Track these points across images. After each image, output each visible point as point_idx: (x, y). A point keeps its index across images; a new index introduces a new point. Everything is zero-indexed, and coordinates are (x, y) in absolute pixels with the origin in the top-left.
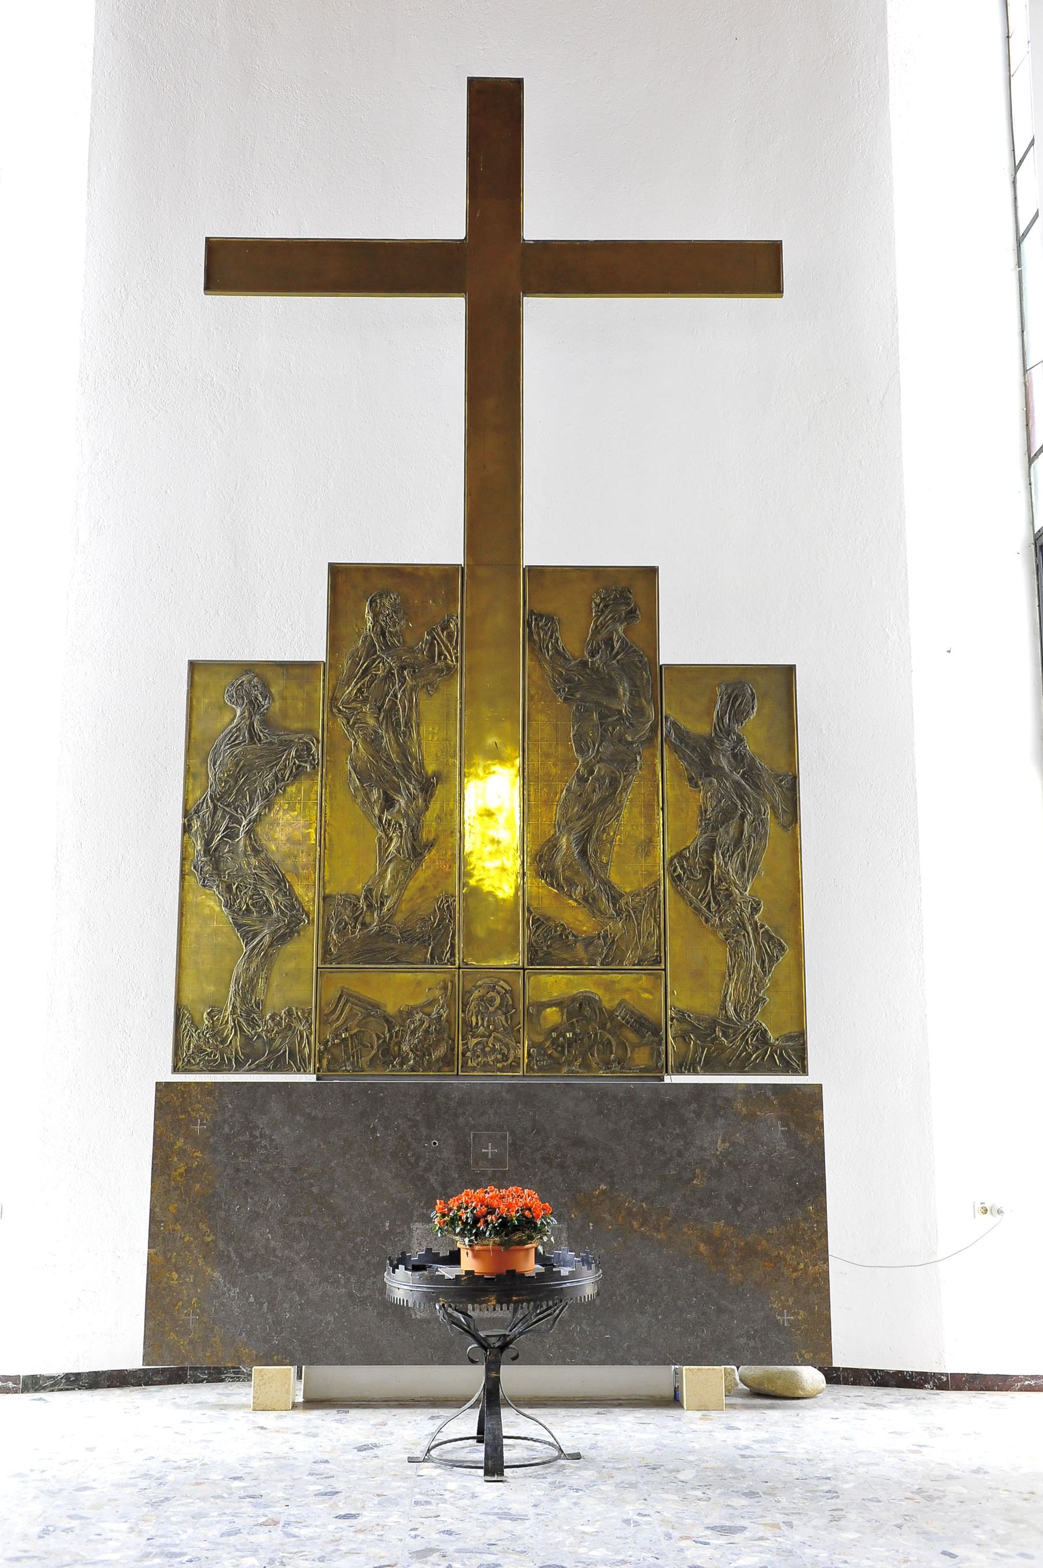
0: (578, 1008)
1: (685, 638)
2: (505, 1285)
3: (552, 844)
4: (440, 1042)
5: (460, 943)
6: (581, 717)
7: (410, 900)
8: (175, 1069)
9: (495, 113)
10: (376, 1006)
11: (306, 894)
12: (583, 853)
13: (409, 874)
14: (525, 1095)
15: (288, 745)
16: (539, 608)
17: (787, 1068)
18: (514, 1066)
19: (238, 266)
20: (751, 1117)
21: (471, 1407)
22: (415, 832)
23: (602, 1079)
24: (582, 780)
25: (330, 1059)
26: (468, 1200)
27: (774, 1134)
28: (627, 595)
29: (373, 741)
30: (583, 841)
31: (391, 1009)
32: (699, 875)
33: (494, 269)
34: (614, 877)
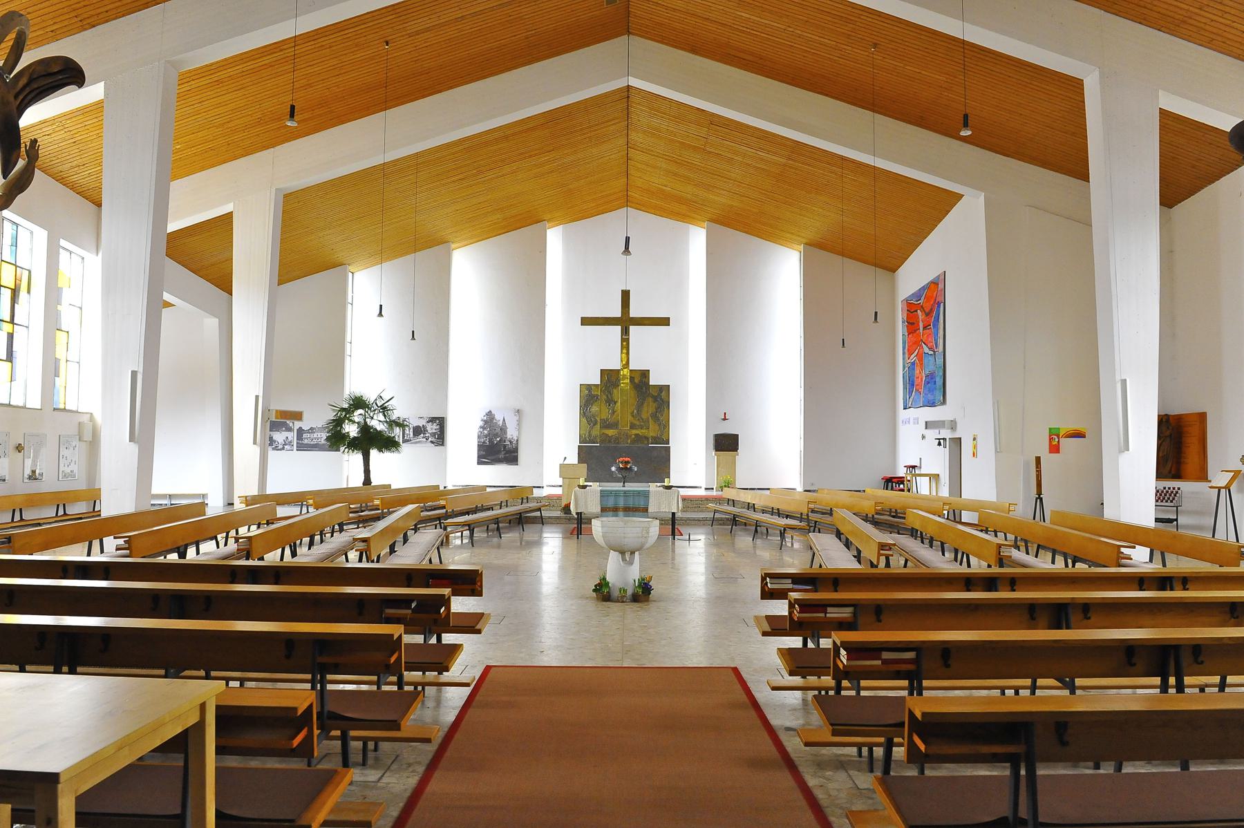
0: (637, 435)
1: (654, 380)
4: (617, 440)
8: (646, 495)
9: (626, 295)
19: (586, 321)
21: (311, 706)
25: (601, 442)
28: (645, 374)
32: (655, 416)
33: (625, 322)
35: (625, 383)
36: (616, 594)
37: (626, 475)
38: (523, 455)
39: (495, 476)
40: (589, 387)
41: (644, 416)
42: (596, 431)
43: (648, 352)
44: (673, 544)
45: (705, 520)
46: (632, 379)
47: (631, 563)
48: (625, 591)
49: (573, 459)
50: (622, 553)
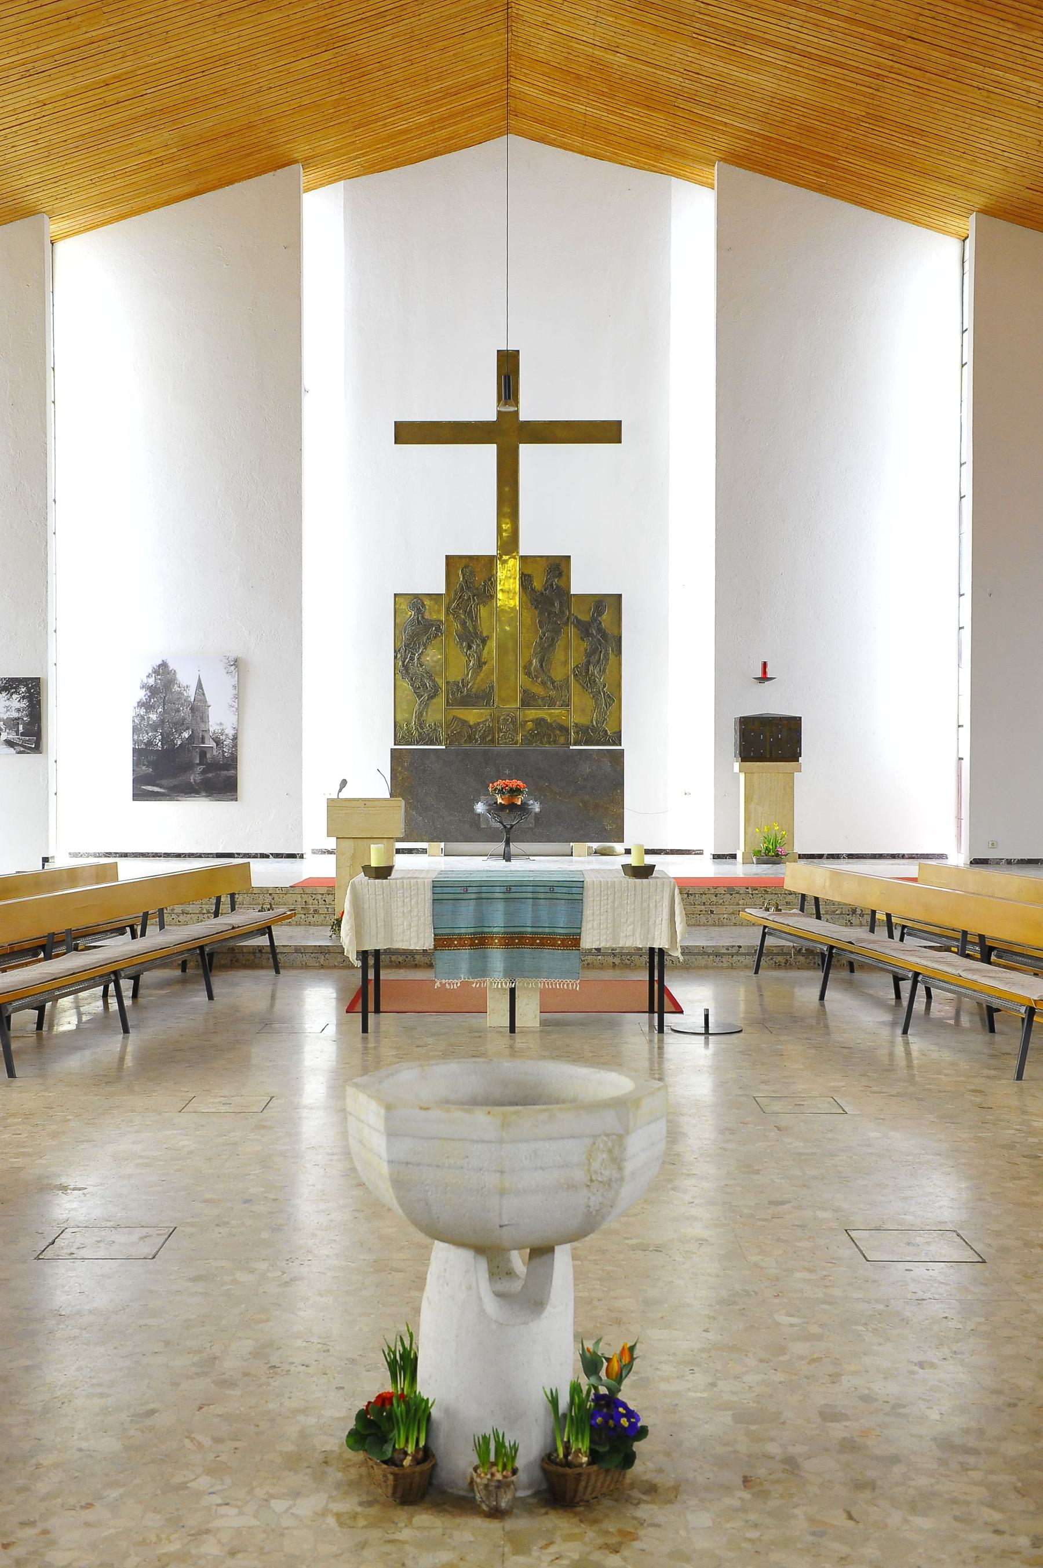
0: (540, 722)
1: (580, 584)
2: (512, 807)
3: (531, 663)
4: (489, 734)
5: (496, 699)
6: (541, 614)
7: (476, 684)
9: (508, 365)
10: (466, 722)
11: (442, 683)
12: (541, 666)
13: (478, 674)
14: (519, 753)
15: (432, 625)
16: (526, 572)
17: (614, 744)
18: (516, 743)
19: (408, 433)
20: (599, 760)
22: (479, 658)
23: (547, 747)
24: (541, 638)
25: (451, 740)
26: (499, 784)
27: (607, 765)
28: (558, 567)
29: (463, 624)
30: (541, 662)
31: (471, 723)
32: (585, 675)
33: (508, 434)
34: (553, 674)
35: (507, 580)
36: (459, 1460)
37: (511, 827)
38: (247, 774)
39: (184, 829)
40: (417, 601)
41: (558, 673)
42: (437, 713)
43: (567, 508)
44: (661, 1041)
45: (735, 951)
46: (525, 580)
47: (532, 1301)
48: (506, 1455)
49: (373, 782)
50: (490, 1251)
